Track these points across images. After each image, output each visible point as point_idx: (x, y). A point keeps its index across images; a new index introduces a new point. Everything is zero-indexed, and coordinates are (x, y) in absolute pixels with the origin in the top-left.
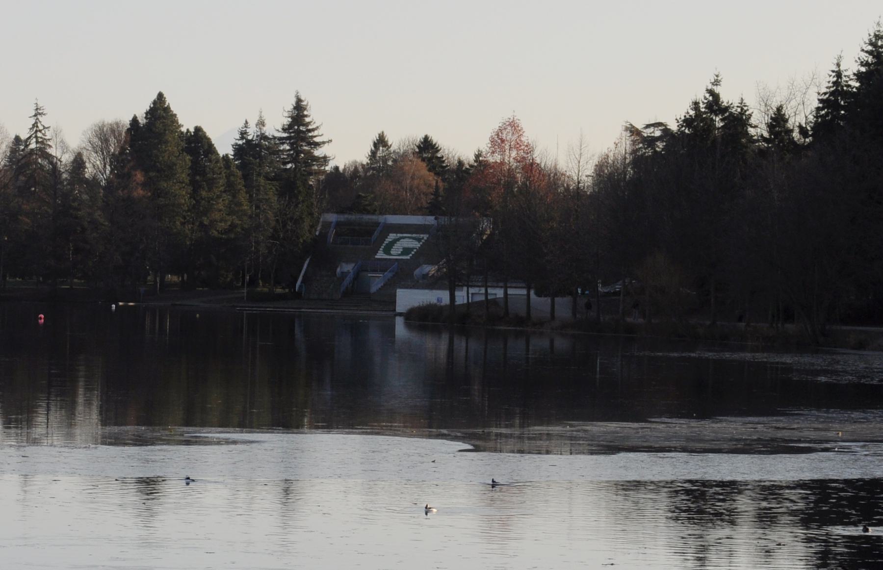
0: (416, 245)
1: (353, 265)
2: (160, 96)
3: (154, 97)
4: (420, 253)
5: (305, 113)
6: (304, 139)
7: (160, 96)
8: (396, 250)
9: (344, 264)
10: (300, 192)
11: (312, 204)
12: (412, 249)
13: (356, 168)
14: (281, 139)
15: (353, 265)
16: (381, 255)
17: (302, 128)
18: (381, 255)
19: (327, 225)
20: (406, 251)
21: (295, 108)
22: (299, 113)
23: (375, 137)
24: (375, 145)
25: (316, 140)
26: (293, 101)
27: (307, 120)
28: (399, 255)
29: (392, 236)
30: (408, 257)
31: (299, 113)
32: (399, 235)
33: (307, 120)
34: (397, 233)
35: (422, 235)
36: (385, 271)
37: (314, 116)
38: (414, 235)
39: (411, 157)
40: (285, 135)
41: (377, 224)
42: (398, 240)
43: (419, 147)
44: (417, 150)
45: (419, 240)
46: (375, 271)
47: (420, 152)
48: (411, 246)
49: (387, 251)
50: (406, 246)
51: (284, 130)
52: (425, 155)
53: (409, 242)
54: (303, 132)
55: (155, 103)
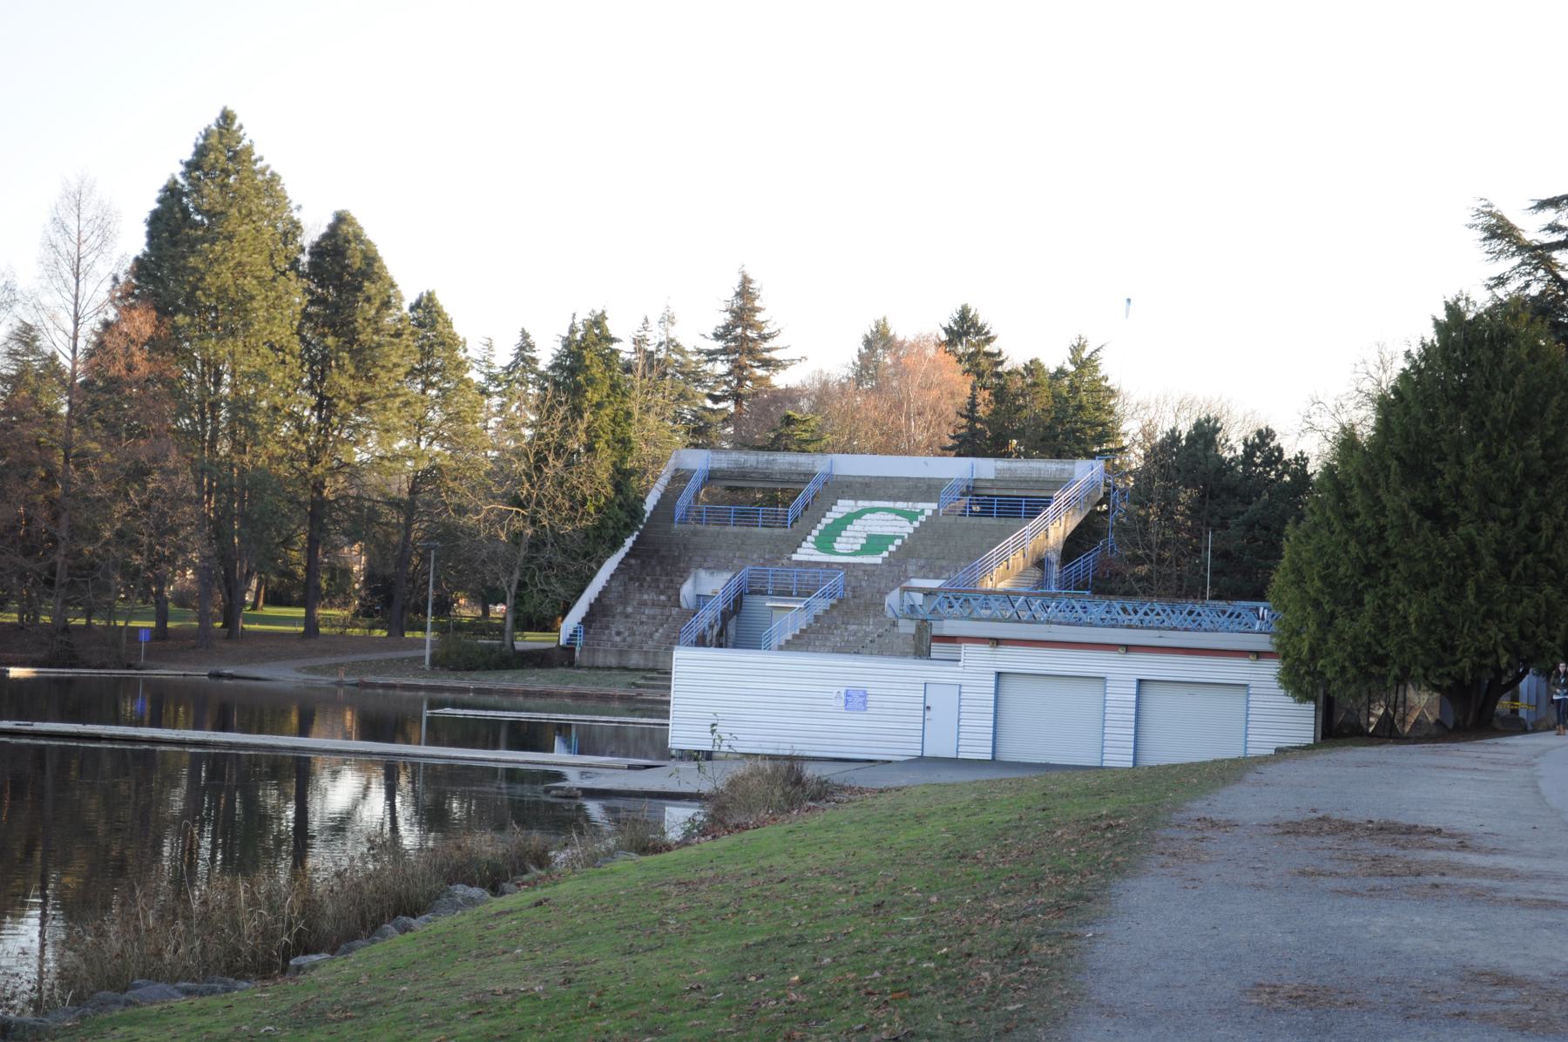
0: (905, 528)
1: (728, 576)
2: (227, 118)
3: (211, 119)
4: (908, 550)
5: (757, 303)
6: (751, 352)
7: (227, 118)
8: (848, 545)
9: (703, 574)
10: (591, 381)
11: (629, 415)
12: (892, 538)
13: (825, 384)
14: (710, 353)
15: (728, 576)
16: (807, 552)
17: (751, 334)
18: (807, 552)
19: (681, 477)
20: (874, 543)
21: (738, 294)
22: (744, 309)
23: (867, 328)
24: (869, 343)
25: (775, 355)
26: (735, 283)
27: (759, 317)
28: (856, 553)
29: (844, 506)
30: (877, 560)
31: (744, 309)
32: (863, 504)
33: (759, 317)
34: (855, 498)
35: (921, 505)
36: (809, 595)
37: (770, 312)
38: (900, 505)
39: (931, 352)
40: (719, 345)
41: (808, 476)
42: (859, 515)
43: (949, 331)
44: (944, 337)
45: (911, 516)
46: (785, 593)
47: (950, 343)
48: (887, 530)
49: (825, 543)
50: (877, 530)
51: (717, 337)
52: (960, 349)
53: (891, 522)
54: (753, 340)
55: (207, 135)
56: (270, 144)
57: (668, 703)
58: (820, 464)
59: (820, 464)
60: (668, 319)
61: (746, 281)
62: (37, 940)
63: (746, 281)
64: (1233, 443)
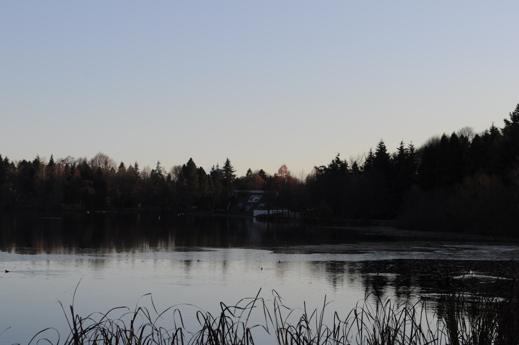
0: (259, 198)
2: (191, 159)
7: (191, 159)
8: (254, 200)
16: (249, 201)
18: (249, 201)
20: (256, 200)
22: (228, 162)
29: (252, 196)
31: (228, 162)
37: (232, 164)
49: (251, 200)
56: (195, 161)
57: (60, 254)
58: (250, 191)
59: (250, 191)
60: (218, 166)
61: (228, 160)
62: (19, 270)
63: (228, 160)
64: (392, 150)
